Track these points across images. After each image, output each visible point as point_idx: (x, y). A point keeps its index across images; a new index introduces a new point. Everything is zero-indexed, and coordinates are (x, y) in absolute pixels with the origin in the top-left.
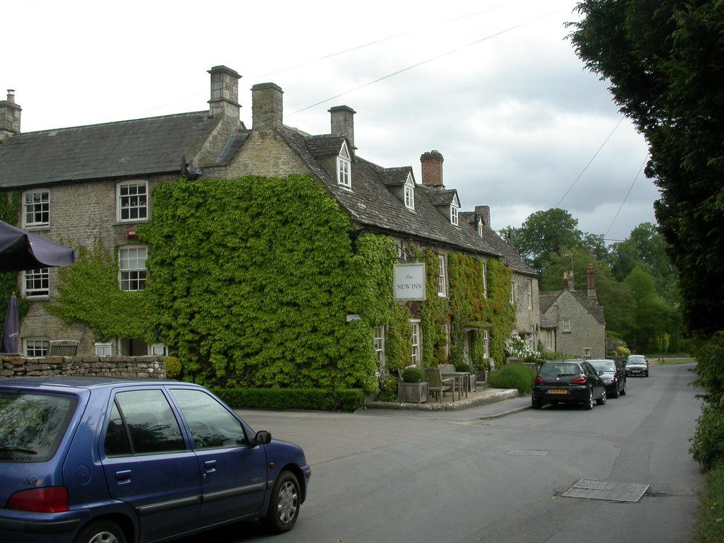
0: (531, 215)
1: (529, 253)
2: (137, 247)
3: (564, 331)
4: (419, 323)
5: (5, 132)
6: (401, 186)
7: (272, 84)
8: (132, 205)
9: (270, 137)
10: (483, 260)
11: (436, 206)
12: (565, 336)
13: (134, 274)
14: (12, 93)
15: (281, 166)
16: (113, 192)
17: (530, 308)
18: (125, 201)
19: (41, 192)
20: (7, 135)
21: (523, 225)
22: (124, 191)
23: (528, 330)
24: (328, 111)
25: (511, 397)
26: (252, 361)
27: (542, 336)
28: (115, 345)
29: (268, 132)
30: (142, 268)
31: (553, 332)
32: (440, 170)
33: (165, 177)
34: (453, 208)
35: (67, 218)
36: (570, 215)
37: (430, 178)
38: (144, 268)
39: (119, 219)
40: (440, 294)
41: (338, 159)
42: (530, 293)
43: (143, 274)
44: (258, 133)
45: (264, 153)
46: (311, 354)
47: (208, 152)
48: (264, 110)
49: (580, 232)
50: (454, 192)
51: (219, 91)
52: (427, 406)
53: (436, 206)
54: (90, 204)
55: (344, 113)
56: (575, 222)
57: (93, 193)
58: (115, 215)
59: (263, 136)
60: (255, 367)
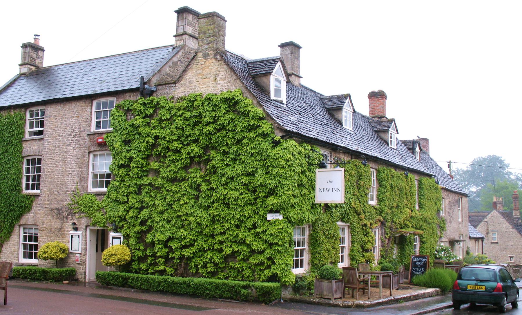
0: (474, 160)
1: (473, 186)
2: (105, 152)
3: (493, 241)
4: (348, 226)
5: (29, 66)
6: (340, 109)
7: (215, 12)
8: (104, 118)
9: (211, 57)
10: (414, 178)
11: (376, 132)
12: (493, 245)
13: (102, 176)
14: (37, 37)
15: (219, 82)
16: (90, 107)
17: (460, 220)
18: (98, 114)
19: (40, 108)
20: (30, 69)
21: (467, 167)
22: (98, 107)
23: (457, 238)
24: (279, 46)
25: (430, 295)
26: (187, 253)
27: (471, 244)
28: (84, 233)
29: (210, 53)
30: (106, 170)
31: (480, 241)
32: (384, 105)
33: (127, 95)
34: (391, 134)
35: (56, 129)
36: (504, 160)
37: (375, 112)
38: (108, 171)
39: (93, 129)
40: (371, 202)
41: (272, 78)
42: (460, 209)
43: (108, 176)
44: (201, 54)
45: (206, 71)
46: (236, 248)
47: (167, 74)
48: (207, 34)
49: (511, 173)
50: (393, 120)
51: (182, 27)
52: (339, 302)
53: (376, 132)
54: (73, 117)
55: (291, 47)
56: (507, 166)
57: (75, 107)
58: (90, 126)
59: (206, 56)
60: (189, 259)
